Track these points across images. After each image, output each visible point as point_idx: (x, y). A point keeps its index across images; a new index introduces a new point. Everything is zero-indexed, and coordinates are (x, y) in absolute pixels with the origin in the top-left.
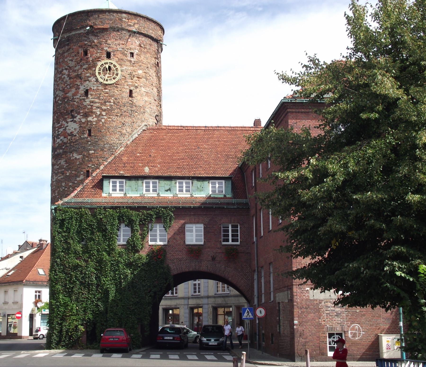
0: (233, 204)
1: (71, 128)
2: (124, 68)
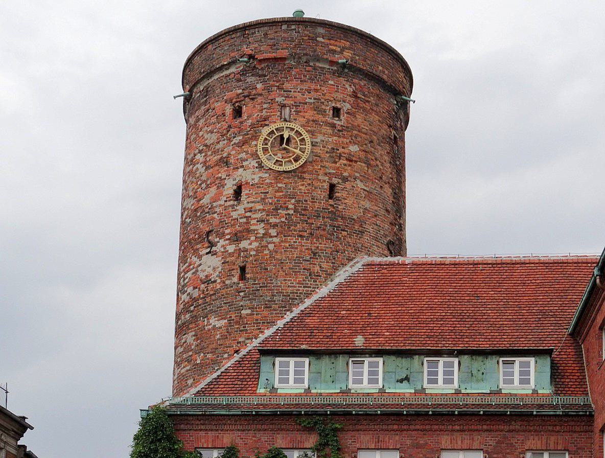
0: (551, 406)
1: (207, 268)
2: (320, 138)
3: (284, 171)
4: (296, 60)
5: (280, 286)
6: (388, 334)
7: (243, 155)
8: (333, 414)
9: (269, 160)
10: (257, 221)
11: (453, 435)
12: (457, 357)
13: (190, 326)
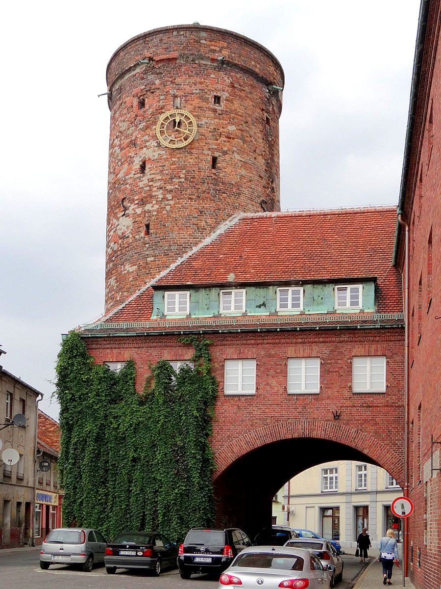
2: (204, 121)
3: (176, 148)
4: (184, 59)
5: (175, 238)
6: (254, 271)
7: (146, 138)
8: (205, 333)
9: (165, 140)
10: (158, 189)
11: (296, 347)
12: (303, 286)
13: (113, 272)
